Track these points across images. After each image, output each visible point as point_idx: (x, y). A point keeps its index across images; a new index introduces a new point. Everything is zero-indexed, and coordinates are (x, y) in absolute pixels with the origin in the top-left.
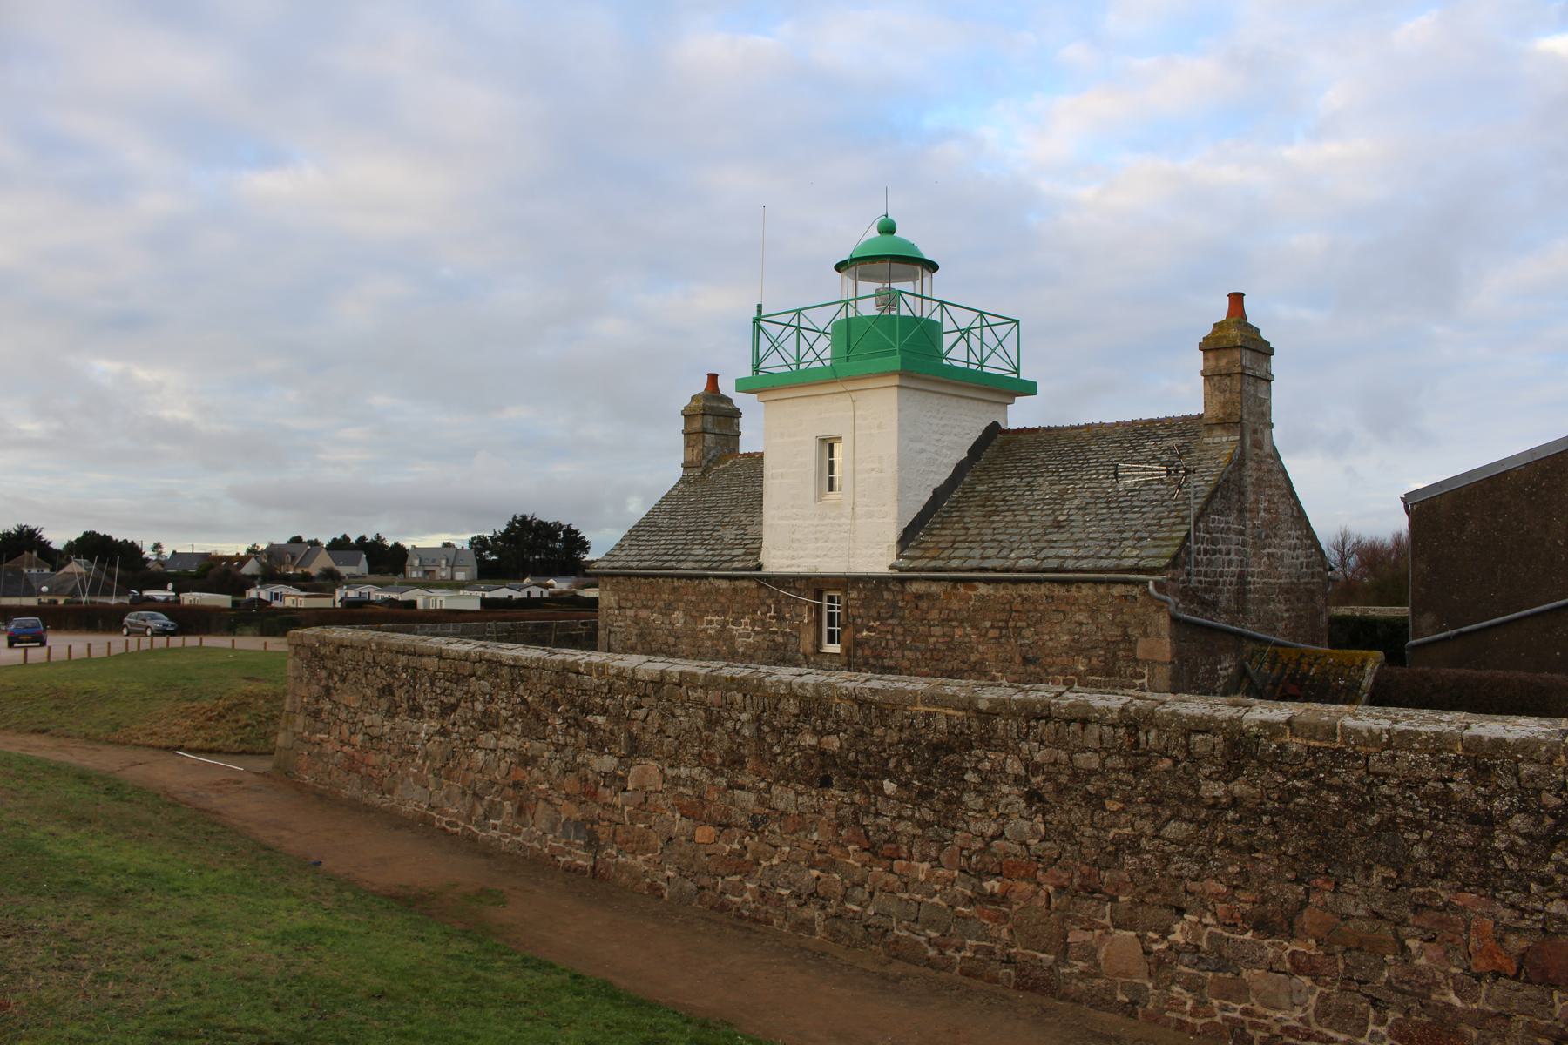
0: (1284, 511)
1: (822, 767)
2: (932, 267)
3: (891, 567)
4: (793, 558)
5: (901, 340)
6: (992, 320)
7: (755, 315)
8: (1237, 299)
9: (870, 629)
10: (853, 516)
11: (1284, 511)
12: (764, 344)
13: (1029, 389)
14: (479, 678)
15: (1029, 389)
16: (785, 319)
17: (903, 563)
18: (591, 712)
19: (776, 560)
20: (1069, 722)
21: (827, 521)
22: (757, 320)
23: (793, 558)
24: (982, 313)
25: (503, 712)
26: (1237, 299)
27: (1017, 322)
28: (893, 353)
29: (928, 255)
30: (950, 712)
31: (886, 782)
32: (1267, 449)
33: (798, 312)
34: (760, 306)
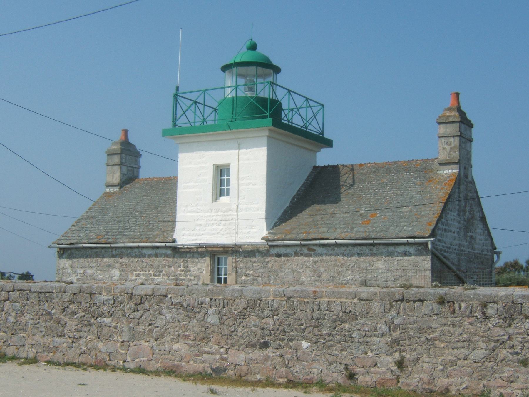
0: (478, 215)
1: (263, 337)
2: (277, 70)
3: (263, 239)
4: (197, 235)
5: (270, 111)
6: (312, 104)
7: (175, 92)
8: (126, 132)
9: (246, 275)
10: (237, 211)
11: (478, 215)
12: (179, 112)
13: (329, 143)
14: (12, 302)
15: (329, 143)
16: (193, 96)
17: (271, 237)
18: (101, 315)
19: (184, 236)
20: (414, 302)
21: (219, 213)
22: (176, 96)
23: (197, 235)
24: (307, 99)
25: (31, 322)
26: (126, 132)
27: (323, 106)
28: (266, 117)
29: (275, 62)
30: (343, 300)
31: (304, 342)
32: (470, 179)
33: (204, 91)
34: (177, 88)
